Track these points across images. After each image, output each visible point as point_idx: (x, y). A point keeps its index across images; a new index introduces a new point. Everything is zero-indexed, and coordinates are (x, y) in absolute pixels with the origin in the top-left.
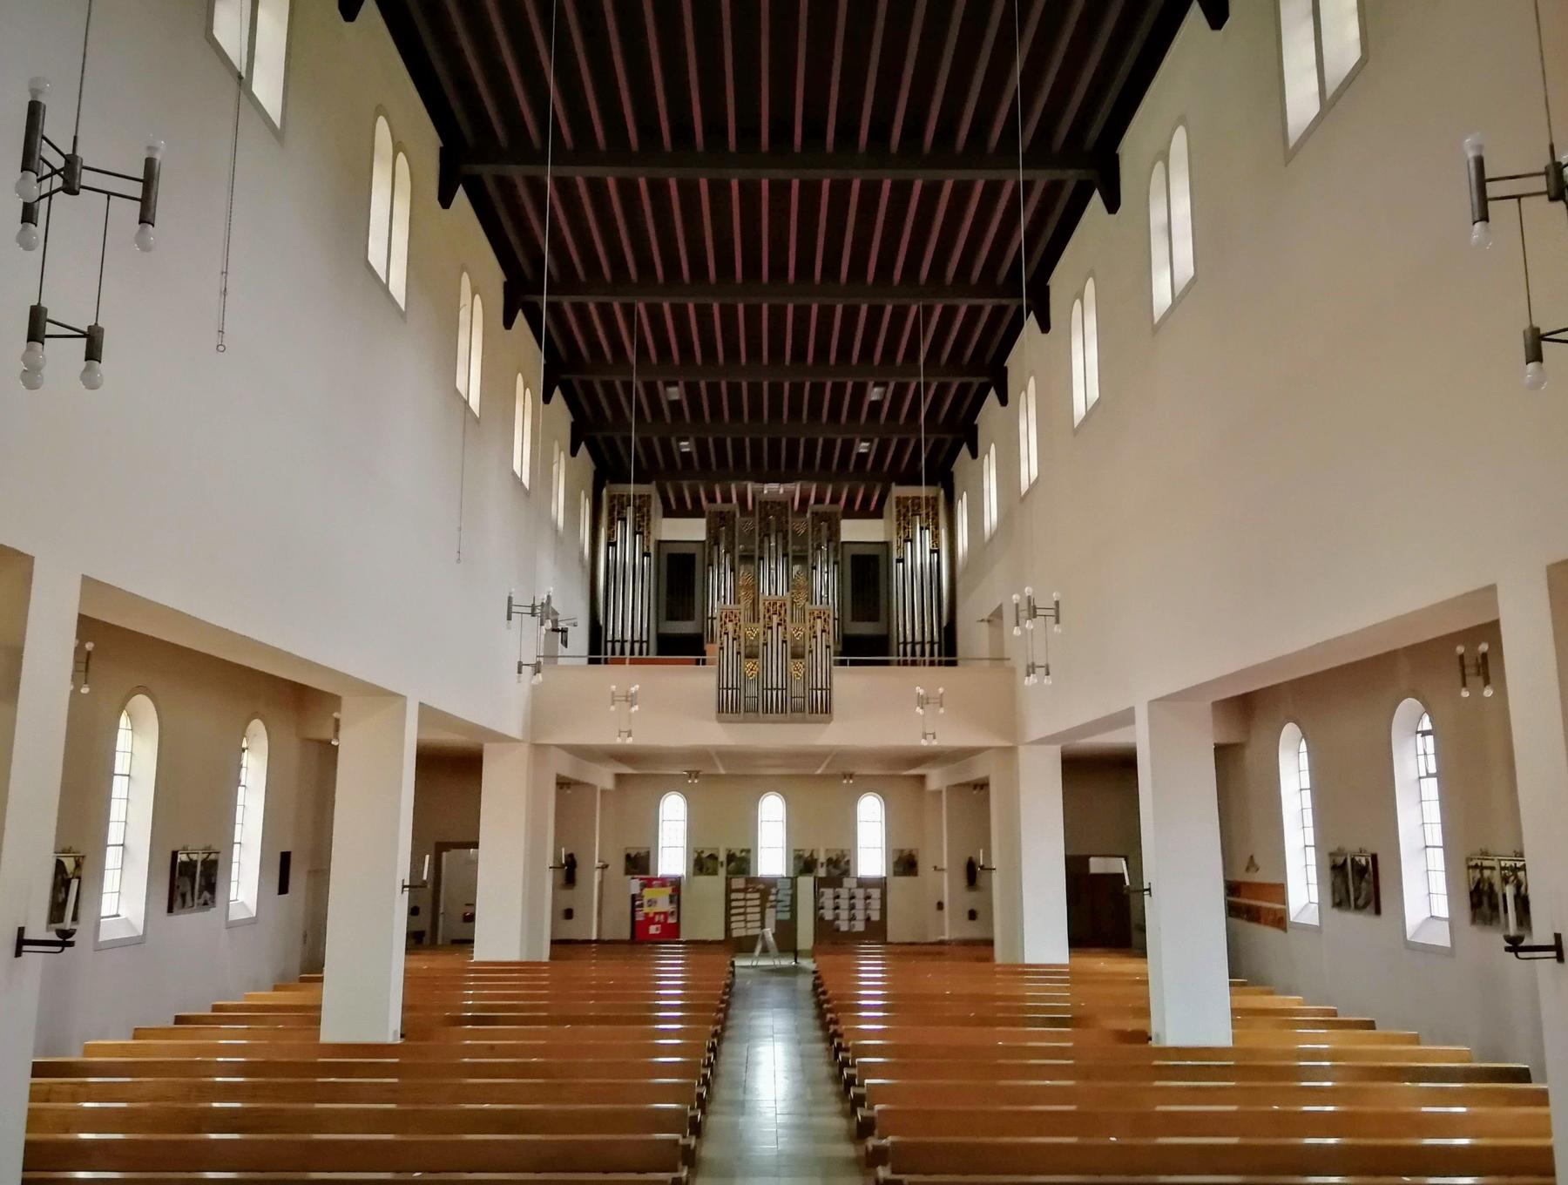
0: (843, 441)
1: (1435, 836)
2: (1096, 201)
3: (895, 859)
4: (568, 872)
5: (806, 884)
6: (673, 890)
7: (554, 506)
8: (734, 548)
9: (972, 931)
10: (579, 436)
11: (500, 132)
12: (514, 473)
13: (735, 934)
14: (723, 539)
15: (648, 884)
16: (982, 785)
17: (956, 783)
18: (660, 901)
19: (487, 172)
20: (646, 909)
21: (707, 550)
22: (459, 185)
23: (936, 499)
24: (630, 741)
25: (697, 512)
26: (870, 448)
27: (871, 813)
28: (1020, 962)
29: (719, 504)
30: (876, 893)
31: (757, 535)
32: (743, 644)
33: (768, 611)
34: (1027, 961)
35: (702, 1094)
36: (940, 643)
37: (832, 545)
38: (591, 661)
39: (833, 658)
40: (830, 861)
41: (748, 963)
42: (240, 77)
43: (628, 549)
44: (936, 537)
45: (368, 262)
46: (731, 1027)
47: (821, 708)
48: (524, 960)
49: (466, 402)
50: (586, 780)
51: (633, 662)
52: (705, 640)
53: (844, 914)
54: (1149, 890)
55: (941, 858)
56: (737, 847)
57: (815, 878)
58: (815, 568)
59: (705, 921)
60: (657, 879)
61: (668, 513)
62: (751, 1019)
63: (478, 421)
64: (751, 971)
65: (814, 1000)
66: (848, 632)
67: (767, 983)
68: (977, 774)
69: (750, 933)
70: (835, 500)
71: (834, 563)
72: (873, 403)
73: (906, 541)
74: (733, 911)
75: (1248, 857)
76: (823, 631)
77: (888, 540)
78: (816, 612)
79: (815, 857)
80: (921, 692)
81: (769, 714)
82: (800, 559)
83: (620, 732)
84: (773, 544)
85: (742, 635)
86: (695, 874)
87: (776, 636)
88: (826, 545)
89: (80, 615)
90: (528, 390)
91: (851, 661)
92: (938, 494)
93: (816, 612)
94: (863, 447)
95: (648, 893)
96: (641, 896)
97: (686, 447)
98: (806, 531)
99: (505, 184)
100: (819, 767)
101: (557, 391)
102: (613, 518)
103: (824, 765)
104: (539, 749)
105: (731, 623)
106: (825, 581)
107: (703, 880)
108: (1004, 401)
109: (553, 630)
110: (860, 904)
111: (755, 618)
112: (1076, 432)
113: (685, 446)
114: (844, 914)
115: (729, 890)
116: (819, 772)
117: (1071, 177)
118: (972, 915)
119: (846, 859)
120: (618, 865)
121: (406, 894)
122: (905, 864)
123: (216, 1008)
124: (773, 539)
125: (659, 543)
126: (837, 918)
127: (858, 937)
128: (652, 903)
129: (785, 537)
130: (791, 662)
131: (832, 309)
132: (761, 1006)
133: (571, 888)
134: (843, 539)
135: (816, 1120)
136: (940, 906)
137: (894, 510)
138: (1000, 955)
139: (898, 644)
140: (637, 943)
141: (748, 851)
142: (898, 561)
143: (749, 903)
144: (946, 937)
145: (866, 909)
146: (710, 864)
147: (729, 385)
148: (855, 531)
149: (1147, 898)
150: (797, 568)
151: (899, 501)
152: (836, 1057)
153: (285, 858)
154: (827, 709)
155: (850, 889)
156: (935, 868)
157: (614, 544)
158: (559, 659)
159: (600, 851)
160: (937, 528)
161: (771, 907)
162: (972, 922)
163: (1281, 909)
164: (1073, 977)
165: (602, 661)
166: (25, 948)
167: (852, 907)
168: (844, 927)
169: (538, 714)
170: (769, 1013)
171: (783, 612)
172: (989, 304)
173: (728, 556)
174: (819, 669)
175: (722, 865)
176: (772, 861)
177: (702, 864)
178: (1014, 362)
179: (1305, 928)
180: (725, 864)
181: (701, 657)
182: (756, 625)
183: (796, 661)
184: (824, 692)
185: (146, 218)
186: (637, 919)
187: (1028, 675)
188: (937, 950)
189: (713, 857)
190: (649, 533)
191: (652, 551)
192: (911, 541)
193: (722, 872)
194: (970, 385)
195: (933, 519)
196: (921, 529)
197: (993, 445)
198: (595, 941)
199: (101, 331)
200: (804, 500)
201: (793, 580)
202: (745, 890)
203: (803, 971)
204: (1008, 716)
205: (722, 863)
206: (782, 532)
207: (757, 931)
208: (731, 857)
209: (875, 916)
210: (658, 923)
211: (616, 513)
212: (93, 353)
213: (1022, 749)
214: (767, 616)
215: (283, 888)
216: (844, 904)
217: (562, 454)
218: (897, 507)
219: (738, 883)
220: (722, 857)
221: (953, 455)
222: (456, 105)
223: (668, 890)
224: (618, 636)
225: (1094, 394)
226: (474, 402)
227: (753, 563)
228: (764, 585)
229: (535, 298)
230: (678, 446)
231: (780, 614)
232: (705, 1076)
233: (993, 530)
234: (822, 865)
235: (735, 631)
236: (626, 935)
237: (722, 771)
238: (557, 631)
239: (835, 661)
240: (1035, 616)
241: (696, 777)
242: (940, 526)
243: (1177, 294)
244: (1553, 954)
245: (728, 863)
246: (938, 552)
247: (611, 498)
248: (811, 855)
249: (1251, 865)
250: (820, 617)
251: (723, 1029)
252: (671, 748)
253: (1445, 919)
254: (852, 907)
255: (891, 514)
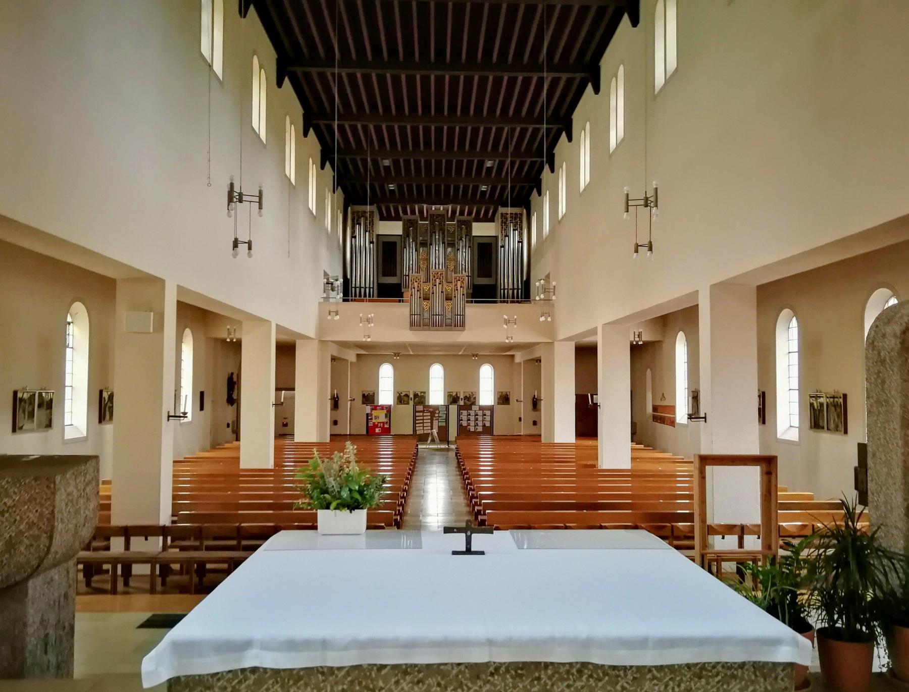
0: (478, 161)
1: (795, 384)
2: (590, 88)
3: (499, 397)
4: (335, 403)
5: (453, 408)
6: (387, 411)
7: (326, 220)
8: (417, 239)
9: (533, 430)
10: (326, 157)
11: (305, 50)
12: (309, 209)
13: (418, 433)
14: (412, 234)
15: (375, 408)
16: (539, 360)
17: (527, 359)
18: (381, 417)
19: (299, 70)
20: (374, 421)
21: (403, 240)
22: (326, 162)
23: (521, 215)
24: (369, 340)
25: (397, 218)
26: (487, 188)
27: (487, 375)
28: (552, 442)
29: (409, 216)
30: (488, 413)
31: (429, 232)
32: (422, 294)
33: (434, 277)
34: (555, 442)
35: (397, 519)
36: (522, 289)
37: (468, 237)
38: (344, 300)
39: (466, 299)
40: (466, 398)
41: (424, 447)
42: (210, 66)
43: (363, 239)
44: (521, 235)
45: (252, 127)
46: (417, 471)
47: (459, 324)
48: (318, 441)
49: (290, 180)
50: (345, 358)
51: (370, 301)
52: (402, 288)
53: (472, 423)
54: (599, 406)
55: (520, 394)
56: (418, 390)
57: (458, 405)
58: (459, 250)
59: (403, 424)
60: (379, 406)
61: (382, 218)
62: (426, 468)
63: (294, 187)
64: (426, 450)
65: (457, 461)
66: (475, 283)
67: (435, 455)
68: (536, 355)
69: (425, 432)
70: (470, 213)
71: (469, 247)
72: (488, 168)
73: (506, 236)
74: (417, 422)
75: (662, 394)
76: (461, 287)
77: (497, 235)
78: (458, 278)
79: (458, 396)
80: (506, 317)
81: (435, 327)
82: (452, 245)
83: (364, 336)
84: (437, 237)
85: (422, 289)
86: (397, 404)
87: (438, 289)
88: (464, 238)
89: (179, 302)
90: (314, 165)
91: (475, 301)
92: (523, 212)
93: (458, 278)
94: (484, 188)
95: (375, 413)
96: (371, 415)
97: (392, 187)
98: (454, 230)
99: (308, 76)
100: (460, 351)
101: (311, 130)
102: (354, 223)
103: (462, 351)
104: (322, 342)
105: (416, 283)
106: (464, 256)
107: (402, 407)
108: (570, 139)
109: (327, 283)
110: (480, 418)
111: (427, 280)
112: (581, 195)
113: (392, 187)
114: (472, 423)
115: (415, 411)
116: (460, 353)
117: (578, 76)
118: (535, 423)
119: (474, 397)
120: (359, 399)
121: (274, 407)
122: (504, 399)
123: (185, 458)
124: (437, 234)
125: (378, 236)
126: (469, 425)
127: (480, 433)
128: (376, 417)
129: (443, 233)
130: (445, 303)
131: (466, 128)
132: (431, 463)
133: (336, 410)
134: (473, 235)
135: (453, 501)
136: (520, 419)
137: (500, 220)
138: (543, 440)
139: (501, 289)
140: (370, 435)
141: (425, 393)
142: (501, 247)
143: (425, 418)
144: (522, 434)
145: (483, 421)
146: (406, 399)
147: (415, 161)
148: (481, 230)
149: (599, 409)
150: (449, 249)
151: (502, 214)
152: (471, 501)
153: (202, 394)
154: (463, 325)
155: (475, 411)
156: (517, 400)
157: (355, 237)
158: (330, 299)
159: (351, 393)
160: (521, 229)
161: (436, 420)
162: (535, 426)
163: (672, 417)
164: (577, 447)
165: (350, 300)
166: (170, 418)
167: (477, 420)
168: (472, 429)
169: (322, 327)
170: (435, 466)
171: (441, 278)
172: (564, 77)
173: (414, 243)
174: (459, 306)
175: (411, 400)
176: (436, 397)
177: (401, 399)
178: (578, 116)
179: (682, 425)
180: (413, 399)
181: (402, 299)
182: (428, 284)
183: (448, 301)
184: (461, 317)
185: (260, 208)
186: (370, 425)
187: (542, 317)
188: (516, 438)
189: (407, 396)
190: (373, 231)
191: (374, 240)
192: (508, 236)
193: (411, 403)
194: (574, 79)
195: (519, 225)
196: (513, 230)
197: (564, 163)
198: (350, 435)
199: (251, 241)
200: (454, 212)
201: (447, 256)
202: (423, 412)
203: (452, 450)
204: (550, 329)
205: (411, 398)
206: (442, 230)
207: (429, 431)
208: (416, 396)
209: (488, 424)
210: (380, 427)
211: (355, 221)
212: (250, 248)
213: (556, 343)
214: (434, 279)
215: (202, 408)
216: (472, 418)
217: (329, 194)
218: (501, 219)
219: (420, 408)
220: (411, 396)
221: (530, 193)
222: (279, 27)
223: (385, 412)
224: (358, 285)
225: (588, 179)
226: (293, 180)
227: (426, 246)
228: (433, 259)
229: (333, 156)
230: (388, 187)
231: (440, 279)
232: (396, 520)
233: (547, 234)
234: (462, 399)
235: (418, 287)
236: (364, 432)
237: (412, 353)
238: (329, 284)
239: (467, 301)
240: (545, 292)
241: (398, 356)
242: (523, 228)
243: (618, 143)
244: (704, 420)
245: (414, 399)
246: (522, 242)
247: (353, 213)
248: (457, 394)
249: (663, 397)
250: (459, 280)
251: (414, 468)
252: (389, 343)
253: (797, 427)
254: (477, 420)
255: (498, 220)
